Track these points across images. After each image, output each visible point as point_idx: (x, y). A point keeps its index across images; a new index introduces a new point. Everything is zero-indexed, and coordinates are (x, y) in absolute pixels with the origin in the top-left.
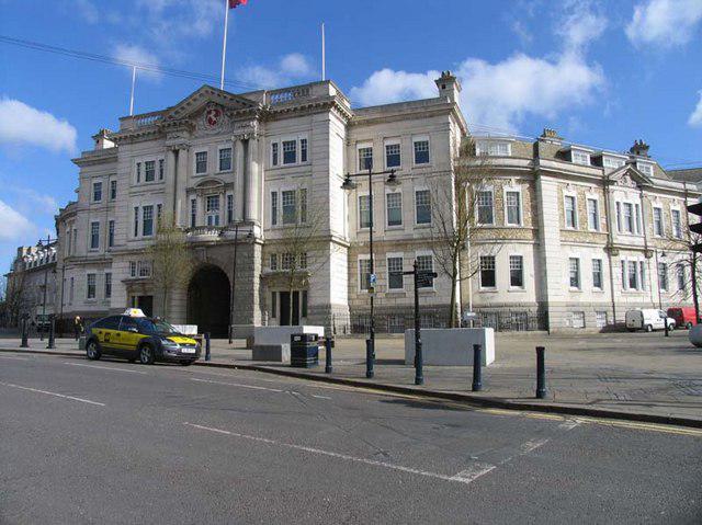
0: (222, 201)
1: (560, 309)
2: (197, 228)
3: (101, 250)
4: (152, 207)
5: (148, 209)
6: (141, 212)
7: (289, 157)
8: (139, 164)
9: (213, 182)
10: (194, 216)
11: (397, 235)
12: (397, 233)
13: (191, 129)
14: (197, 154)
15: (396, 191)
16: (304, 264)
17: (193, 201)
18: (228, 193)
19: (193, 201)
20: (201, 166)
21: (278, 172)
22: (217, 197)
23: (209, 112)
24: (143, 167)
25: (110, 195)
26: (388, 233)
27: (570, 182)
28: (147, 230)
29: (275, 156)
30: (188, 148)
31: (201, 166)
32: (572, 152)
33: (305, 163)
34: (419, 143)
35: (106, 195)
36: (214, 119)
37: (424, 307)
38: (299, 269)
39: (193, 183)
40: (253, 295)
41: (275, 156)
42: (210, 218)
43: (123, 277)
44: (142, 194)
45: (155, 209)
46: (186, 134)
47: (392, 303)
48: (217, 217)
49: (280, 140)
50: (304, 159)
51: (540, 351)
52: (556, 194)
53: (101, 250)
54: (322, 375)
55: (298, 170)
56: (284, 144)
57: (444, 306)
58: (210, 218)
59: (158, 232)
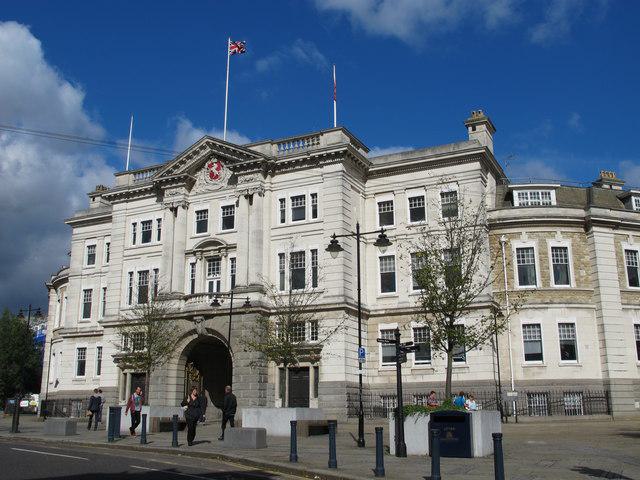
0: (225, 264)
1: (625, 388)
2: (196, 296)
3: (93, 322)
4: (303, 253)
5: (144, 274)
6: (136, 277)
7: (299, 214)
8: (135, 224)
9: (215, 243)
10: (193, 281)
11: (391, 302)
12: (392, 301)
13: (190, 184)
14: (197, 212)
15: (387, 254)
16: (315, 336)
17: (193, 265)
18: (230, 255)
19: (193, 265)
20: (202, 226)
21: (285, 231)
22: (220, 259)
23: (211, 166)
24: (139, 228)
25: (105, 257)
26: (382, 302)
27: (630, 233)
28: (143, 298)
29: (283, 212)
30: (185, 207)
31: (202, 226)
32: (633, 198)
33: (316, 219)
34: (415, 199)
35: (100, 258)
36: (216, 172)
37: (411, 385)
38: (309, 341)
39: (191, 245)
40: (308, 382)
41: (283, 212)
42: (211, 284)
43: (115, 351)
44: (136, 257)
45: (309, 256)
46: (183, 190)
47: (419, 380)
48: (219, 283)
49: (288, 195)
50: (315, 215)
51: (99, 373)
52: (613, 248)
53: (93, 322)
54: (284, 465)
55: (310, 227)
56: (293, 198)
57: (439, 384)
58: (211, 284)
59: (154, 300)
